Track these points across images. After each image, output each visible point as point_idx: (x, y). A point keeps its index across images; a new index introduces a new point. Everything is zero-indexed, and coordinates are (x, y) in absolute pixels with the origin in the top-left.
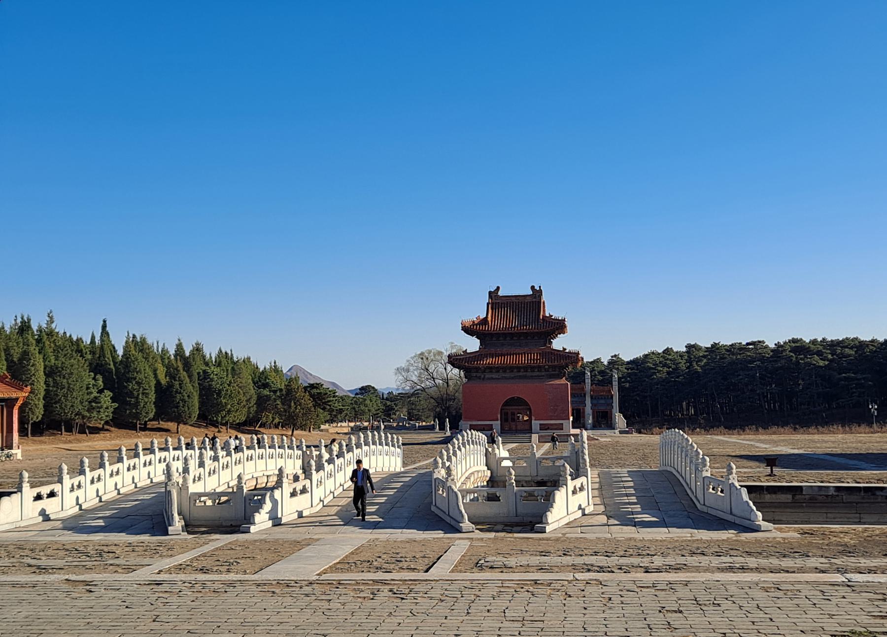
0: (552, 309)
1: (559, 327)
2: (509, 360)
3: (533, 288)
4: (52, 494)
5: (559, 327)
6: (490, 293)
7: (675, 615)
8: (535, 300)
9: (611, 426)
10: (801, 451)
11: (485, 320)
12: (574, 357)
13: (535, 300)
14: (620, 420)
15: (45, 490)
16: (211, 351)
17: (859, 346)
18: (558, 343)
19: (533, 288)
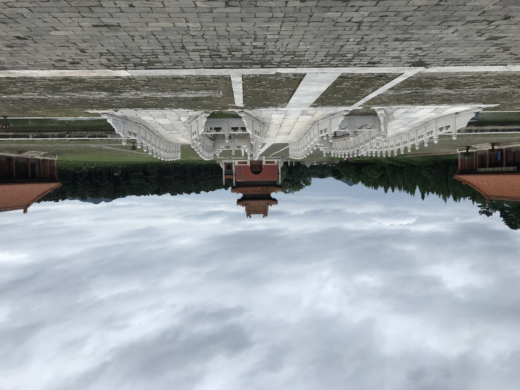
0: (242, 209)
1: (239, 202)
2: (440, 214)
3: (250, 217)
4: (441, 129)
5: (239, 202)
6: (267, 215)
7: (165, 40)
8: (249, 214)
9: (226, 164)
10: (244, 180)
11: (268, 204)
12: (234, 189)
13: (249, 214)
14: (223, 167)
15: (444, 131)
16: (381, 189)
17: (83, 199)
18: (240, 195)
19: (250, 217)
